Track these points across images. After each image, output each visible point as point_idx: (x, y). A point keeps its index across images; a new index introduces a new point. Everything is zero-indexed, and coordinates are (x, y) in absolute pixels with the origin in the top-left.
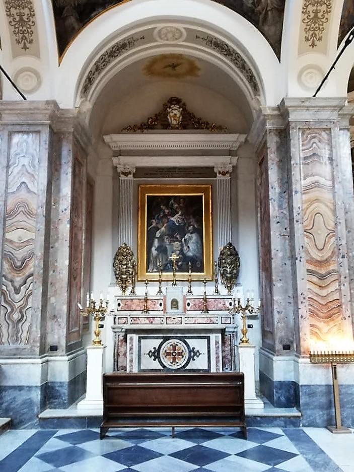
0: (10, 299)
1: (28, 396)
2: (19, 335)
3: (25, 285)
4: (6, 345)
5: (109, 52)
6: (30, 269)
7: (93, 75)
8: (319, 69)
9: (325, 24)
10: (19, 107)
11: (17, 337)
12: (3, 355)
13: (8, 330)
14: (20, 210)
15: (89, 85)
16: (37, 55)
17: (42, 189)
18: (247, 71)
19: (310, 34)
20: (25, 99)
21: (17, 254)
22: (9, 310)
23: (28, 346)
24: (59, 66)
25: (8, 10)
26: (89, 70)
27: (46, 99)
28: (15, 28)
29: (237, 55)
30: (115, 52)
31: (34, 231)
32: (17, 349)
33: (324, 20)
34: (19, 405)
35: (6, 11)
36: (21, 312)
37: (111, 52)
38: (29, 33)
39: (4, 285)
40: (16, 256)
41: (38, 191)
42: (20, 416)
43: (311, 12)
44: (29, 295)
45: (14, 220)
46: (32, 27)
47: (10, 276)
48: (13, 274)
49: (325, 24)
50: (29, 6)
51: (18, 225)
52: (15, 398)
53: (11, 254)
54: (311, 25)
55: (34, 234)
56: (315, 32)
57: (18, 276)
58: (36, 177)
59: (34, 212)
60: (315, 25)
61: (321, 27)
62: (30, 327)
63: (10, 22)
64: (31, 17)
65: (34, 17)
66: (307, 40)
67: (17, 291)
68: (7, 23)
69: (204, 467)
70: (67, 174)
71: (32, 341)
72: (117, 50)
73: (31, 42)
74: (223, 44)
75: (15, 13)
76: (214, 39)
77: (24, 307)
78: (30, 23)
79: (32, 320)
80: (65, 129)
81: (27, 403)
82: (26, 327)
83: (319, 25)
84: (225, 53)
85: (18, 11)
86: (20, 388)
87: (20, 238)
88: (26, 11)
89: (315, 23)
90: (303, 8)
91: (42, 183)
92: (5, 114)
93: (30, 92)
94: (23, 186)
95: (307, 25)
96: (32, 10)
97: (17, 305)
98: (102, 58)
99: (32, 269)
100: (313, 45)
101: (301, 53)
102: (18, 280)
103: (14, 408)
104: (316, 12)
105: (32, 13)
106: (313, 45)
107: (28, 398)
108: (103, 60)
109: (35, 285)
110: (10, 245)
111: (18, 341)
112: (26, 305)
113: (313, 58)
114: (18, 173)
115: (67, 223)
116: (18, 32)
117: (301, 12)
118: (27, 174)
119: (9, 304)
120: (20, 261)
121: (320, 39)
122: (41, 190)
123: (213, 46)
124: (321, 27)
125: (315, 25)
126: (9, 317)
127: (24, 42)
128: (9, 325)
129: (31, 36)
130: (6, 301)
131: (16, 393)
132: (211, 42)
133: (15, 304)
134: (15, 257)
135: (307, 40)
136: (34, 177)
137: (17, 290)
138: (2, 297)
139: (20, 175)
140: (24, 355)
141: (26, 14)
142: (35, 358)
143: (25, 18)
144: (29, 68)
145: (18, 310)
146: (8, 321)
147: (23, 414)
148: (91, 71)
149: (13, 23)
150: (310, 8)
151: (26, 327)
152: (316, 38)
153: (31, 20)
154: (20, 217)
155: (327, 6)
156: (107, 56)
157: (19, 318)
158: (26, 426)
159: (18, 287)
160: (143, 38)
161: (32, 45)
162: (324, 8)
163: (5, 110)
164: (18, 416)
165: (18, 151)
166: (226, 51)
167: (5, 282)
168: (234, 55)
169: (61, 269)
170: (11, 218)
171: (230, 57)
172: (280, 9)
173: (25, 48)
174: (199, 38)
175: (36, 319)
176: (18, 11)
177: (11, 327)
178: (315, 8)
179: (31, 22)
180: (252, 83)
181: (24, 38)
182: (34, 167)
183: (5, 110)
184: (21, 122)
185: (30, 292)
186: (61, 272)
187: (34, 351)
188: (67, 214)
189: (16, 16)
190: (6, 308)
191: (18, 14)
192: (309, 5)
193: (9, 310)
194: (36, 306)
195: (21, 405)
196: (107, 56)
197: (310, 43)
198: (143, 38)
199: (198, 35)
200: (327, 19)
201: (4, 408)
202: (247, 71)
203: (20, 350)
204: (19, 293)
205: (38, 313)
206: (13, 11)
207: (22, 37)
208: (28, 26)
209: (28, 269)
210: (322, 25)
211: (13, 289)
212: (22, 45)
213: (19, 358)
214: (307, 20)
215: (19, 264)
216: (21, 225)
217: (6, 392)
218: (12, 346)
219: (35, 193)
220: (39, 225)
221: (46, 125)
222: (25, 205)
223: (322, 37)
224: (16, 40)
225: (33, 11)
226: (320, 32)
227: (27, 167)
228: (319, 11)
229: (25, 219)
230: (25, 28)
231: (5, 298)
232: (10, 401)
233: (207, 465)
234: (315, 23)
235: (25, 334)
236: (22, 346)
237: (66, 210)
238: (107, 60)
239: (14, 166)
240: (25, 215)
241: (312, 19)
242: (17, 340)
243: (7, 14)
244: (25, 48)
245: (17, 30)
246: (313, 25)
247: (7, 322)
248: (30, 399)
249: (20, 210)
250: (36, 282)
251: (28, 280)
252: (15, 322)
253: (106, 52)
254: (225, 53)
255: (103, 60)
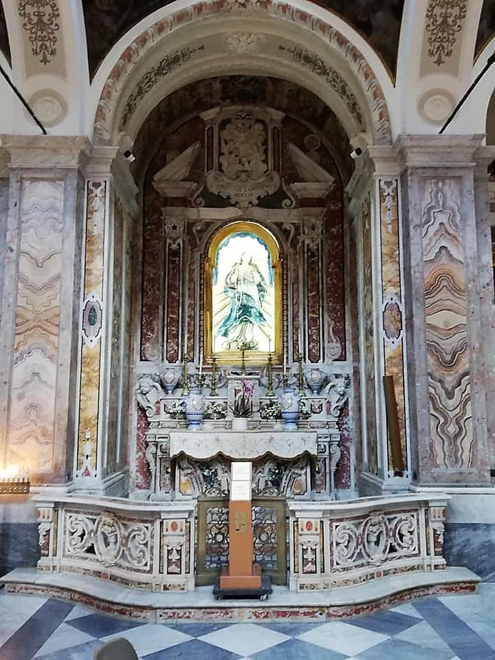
0: (441, 406)
1: (487, 537)
2: (459, 455)
3: (459, 387)
4: (443, 467)
5: (156, 68)
6: (464, 365)
7: (135, 100)
8: (450, 96)
9: (456, 33)
10: (436, 143)
11: (456, 458)
12: (442, 482)
13: (443, 448)
14: (443, 284)
15: (129, 115)
16: (62, 72)
17: (472, 256)
18: (348, 96)
19: (436, 47)
20: (45, 133)
21: (444, 345)
22: (442, 421)
23: (474, 470)
24: (395, 87)
25: (430, 9)
26: (128, 93)
27: (473, 133)
28: (32, 33)
29: (335, 74)
30: (164, 69)
31: (465, 313)
32: (461, 473)
33: (456, 28)
34: (476, 550)
35: (19, 9)
36: (458, 423)
37: (159, 67)
38: (51, 40)
39: (432, 387)
40: (443, 347)
41: (466, 258)
42: (478, 565)
43: (438, 16)
44: (467, 401)
45: (436, 298)
46: (55, 32)
47: (437, 375)
48: (441, 371)
49: (456, 33)
50: (461, 5)
51: (442, 305)
52: (468, 540)
53: (436, 345)
54: (438, 33)
55: (465, 317)
56: (443, 44)
57: (449, 375)
58: (460, 239)
59: (463, 288)
60: (42, 33)
61: (451, 37)
62: (473, 445)
63: (25, 25)
64: (458, 20)
65: (58, 18)
66: (431, 54)
67: (450, 395)
68: (424, 26)
69: (101, 639)
70: (485, 236)
71: (479, 462)
72: (167, 66)
73: (53, 53)
74: (316, 60)
75: (438, 14)
76: (303, 53)
77: (462, 417)
78: (53, 26)
79: (475, 434)
80: (479, 174)
81: (486, 547)
82: (467, 444)
83: (449, 34)
84: (319, 71)
85: (35, 9)
86: (475, 527)
87: (446, 324)
88: (48, 10)
89: (443, 31)
90: (428, 11)
91: (471, 248)
92: (413, 153)
93: (52, 124)
94: (443, 251)
95: (432, 34)
96: (55, 8)
97: (452, 414)
98: (147, 77)
99: (467, 366)
100: (439, 62)
101: (424, 72)
102: (450, 380)
103: (469, 554)
104: (445, 17)
105: (56, 13)
106: (439, 62)
107: (486, 540)
108: (147, 79)
109: (476, 387)
110: (435, 333)
111: (458, 463)
112: (464, 414)
113: (440, 80)
114: (435, 235)
115: (491, 303)
116: (36, 39)
117: (425, 14)
118: (447, 235)
119: (441, 413)
120: (449, 354)
121: (449, 54)
122: (471, 258)
123: (302, 61)
124: (451, 37)
125: (42, 33)
126: (443, 431)
127: (44, 52)
128: (444, 442)
129: (54, 44)
130: (436, 409)
131: (470, 534)
132: (300, 54)
133: (449, 412)
134: (442, 349)
135: (431, 54)
136: (457, 240)
137: (450, 393)
138: (431, 403)
139: (438, 237)
140: (471, 482)
141: (453, 16)
142: (487, 487)
143: (45, 19)
144: (429, 91)
145: (454, 419)
146: (442, 436)
147: (483, 561)
148: (132, 96)
149: (29, 26)
150: (438, 11)
151: (467, 444)
152: (48, 51)
153: (54, 23)
154: (444, 294)
155: (461, 9)
156: (153, 74)
157: (456, 432)
158: (488, 577)
159: (450, 389)
160: (202, 48)
161: (55, 57)
162: (456, 11)
163: (413, 147)
164: (475, 566)
165: (433, 204)
166: (319, 68)
167: (432, 383)
168: (331, 74)
169: (490, 366)
170: (431, 296)
171: (325, 77)
172: (397, 11)
173: (45, 61)
174: (283, 49)
175: (481, 434)
176: (35, 9)
177: (446, 444)
178: (444, 10)
179: (54, 25)
180: (355, 114)
181: (44, 47)
182: (456, 226)
183: (413, 147)
184: (436, 164)
185: (467, 397)
186: (490, 369)
187: (484, 476)
188: (490, 290)
189: (32, 17)
190: (437, 418)
191: (36, 14)
192: (437, 7)
193: (442, 421)
194: (480, 415)
195: (480, 549)
196: (153, 74)
197: (435, 58)
198: (202, 48)
199: (283, 46)
200: (56, 25)
201: (456, 553)
202: (348, 96)
203: (464, 475)
204: (453, 398)
205: (484, 425)
206: (29, 9)
207: (41, 47)
208: (50, 31)
209: (461, 365)
210: (53, 33)
211: (443, 391)
212: (41, 57)
213: (466, 486)
214: (432, 27)
215: (448, 358)
216: (446, 306)
217: (457, 532)
218: (451, 470)
219: (461, 262)
220: (472, 306)
221: (469, 168)
222: (447, 275)
223: (451, 51)
224: (430, 50)
225: (57, 10)
226: (450, 45)
227: (447, 226)
228: (449, 15)
229: (450, 297)
230: (45, 33)
231: (434, 405)
232: (463, 544)
233: (204, 636)
234: (443, 31)
235: (466, 453)
236: (464, 469)
237: (488, 284)
238: (153, 80)
239: (429, 224)
240: (450, 291)
241: (439, 25)
242: (457, 461)
243: (20, 14)
244: (45, 61)
245: (34, 36)
246: (440, 34)
247: (440, 436)
248: (489, 541)
249: (443, 284)
250: (476, 383)
251: (462, 381)
252: (452, 436)
253: (153, 68)
254: (319, 71)
255: (147, 79)
